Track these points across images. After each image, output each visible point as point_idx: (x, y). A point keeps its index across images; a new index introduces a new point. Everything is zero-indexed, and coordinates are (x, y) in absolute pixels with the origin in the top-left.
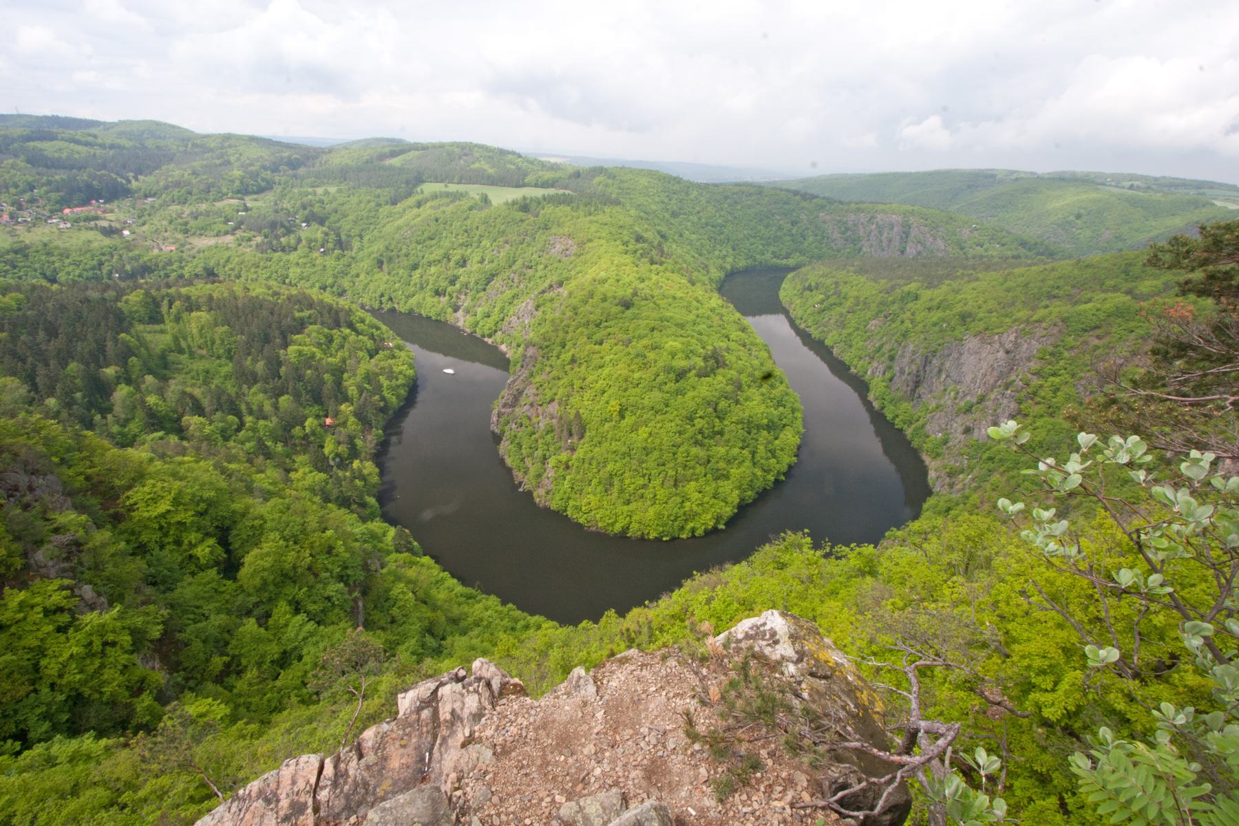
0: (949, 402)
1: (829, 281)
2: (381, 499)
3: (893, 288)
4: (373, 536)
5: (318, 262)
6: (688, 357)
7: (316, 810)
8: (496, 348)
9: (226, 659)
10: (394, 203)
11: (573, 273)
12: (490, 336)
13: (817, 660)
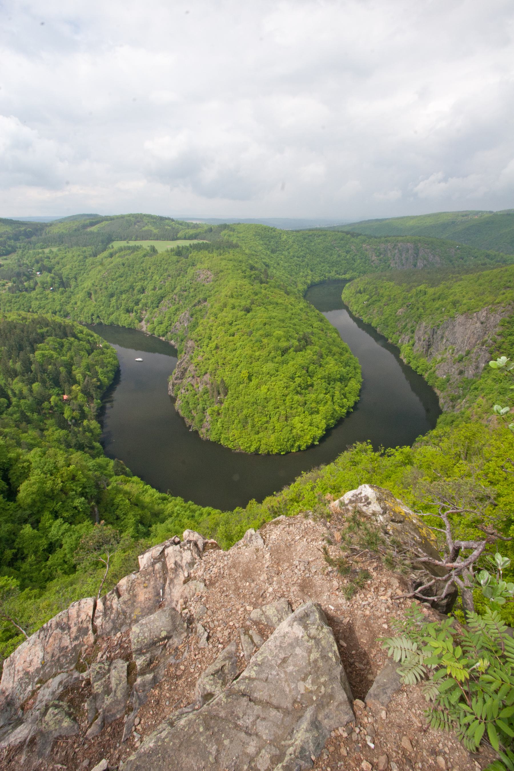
0: (449, 356)
1: (371, 287)
2: (102, 443)
3: (411, 288)
4: (100, 467)
5: (49, 296)
6: (288, 340)
7: (95, 631)
8: (168, 343)
9: (14, 551)
10: (95, 255)
11: (213, 292)
12: (163, 336)
13: (394, 512)
